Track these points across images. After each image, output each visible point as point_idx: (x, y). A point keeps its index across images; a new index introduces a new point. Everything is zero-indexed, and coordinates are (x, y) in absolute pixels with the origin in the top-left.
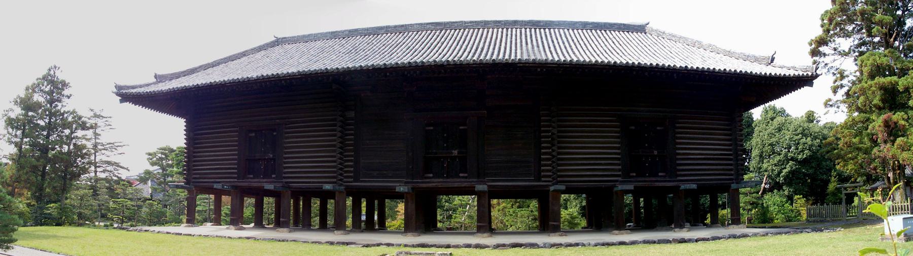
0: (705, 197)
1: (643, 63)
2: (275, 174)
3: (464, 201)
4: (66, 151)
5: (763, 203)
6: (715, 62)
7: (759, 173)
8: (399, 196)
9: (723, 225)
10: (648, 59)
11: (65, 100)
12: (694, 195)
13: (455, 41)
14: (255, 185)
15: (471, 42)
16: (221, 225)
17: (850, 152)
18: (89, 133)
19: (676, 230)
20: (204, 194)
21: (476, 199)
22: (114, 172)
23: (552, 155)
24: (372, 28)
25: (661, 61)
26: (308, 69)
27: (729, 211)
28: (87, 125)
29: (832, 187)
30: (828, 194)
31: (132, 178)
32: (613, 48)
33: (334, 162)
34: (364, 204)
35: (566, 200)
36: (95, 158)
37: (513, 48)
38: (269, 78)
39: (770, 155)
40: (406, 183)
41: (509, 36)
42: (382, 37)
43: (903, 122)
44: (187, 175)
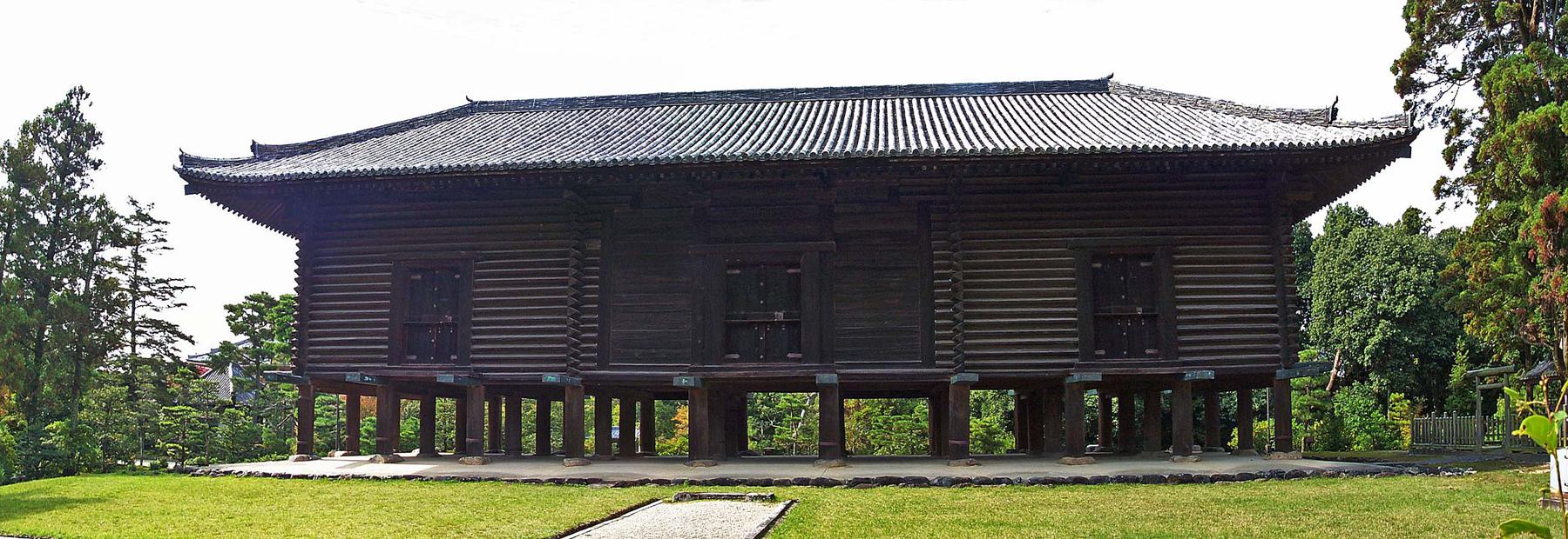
0: (1229, 395)
1: (1110, 146)
3: (795, 402)
4: (82, 293)
5: (1333, 409)
6: (1235, 133)
7: (1326, 346)
8: (681, 394)
9: (1261, 452)
10: (1118, 139)
11: (90, 171)
12: (1208, 390)
13: (779, 121)
14: (421, 374)
15: (808, 123)
16: (360, 454)
17: (1489, 295)
18: (125, 253)
19: (1176, 458)
21: (818, 398)
22: (167, 345)
23: (954, 319)
24: (636, 96)
25: (1142, 141)
26: (523, 160)
27: (1272, 423)
28: (123, 235)
29: (1457, 373)
30: (1449, 392)
31: (199, 359)
32: (1055, 124)
33: (564, 331)
34: (616, 409)
35: (979, 401)
36: (133, 313)
37: (882, 132)
38: (453, 172)
39: (1345, 308)
40: (691, 370)
41: (874, 112)
42: (654, 112)
44: (299, 353)
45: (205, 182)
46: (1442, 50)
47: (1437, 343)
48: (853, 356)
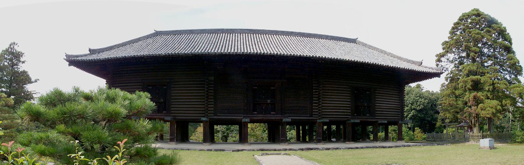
2: (165, 111)
30: (436, 128)
43: (482, 97)
46: (449, 55)
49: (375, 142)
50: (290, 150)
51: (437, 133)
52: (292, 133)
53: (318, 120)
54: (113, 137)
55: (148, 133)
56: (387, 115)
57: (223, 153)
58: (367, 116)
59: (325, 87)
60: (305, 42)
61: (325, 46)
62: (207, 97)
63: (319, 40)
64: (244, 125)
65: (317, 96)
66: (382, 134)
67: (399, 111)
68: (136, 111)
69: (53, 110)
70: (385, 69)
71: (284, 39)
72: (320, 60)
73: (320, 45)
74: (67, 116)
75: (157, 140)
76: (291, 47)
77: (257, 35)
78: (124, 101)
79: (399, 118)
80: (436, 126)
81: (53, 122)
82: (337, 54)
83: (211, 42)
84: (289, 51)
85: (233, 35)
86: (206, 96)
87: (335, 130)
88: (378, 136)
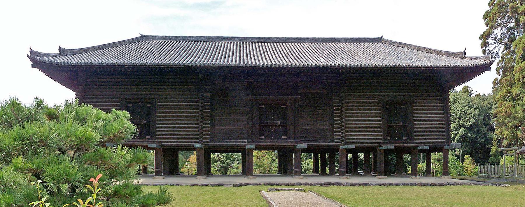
2: (149, 135)
20: (361, 147)
45: (43, 63)
47: (480, 137)
48: (305, 138)
49: (413, 177)
50: (306, 184)
51: (492, 164)
52: (308, 163)
53: (341, 147)
54: (84, 173)
55: (128, 165)
56: (429, 137)
57: (221, 188)
58: (403, 140)
59: (348, 103)
60: (321, 49)
61: (345, 51)
62: (202, 118)
63: (338, 45)
64: (248, 153)
65: (339, 115)
66: (422, 166)
67: (444, 130)
68: (112, 136)
69: (9, 133)
70: (421, 71)
71: (295, 47)
72: (340, 69)
73: (339, 51)
74: (26, 142)
75: (139, 174)
76: (304, 56)
77: (263, 44)
78: (97, 123)
79: (443, 142)
80: (491, 153)
81: (8, 152)
82: (360, 59)
83: (207, 52)
84: (301, 61)
85: (234, 44)
86: (200, 116)
87: (363, 159)
88: (418, 168)
